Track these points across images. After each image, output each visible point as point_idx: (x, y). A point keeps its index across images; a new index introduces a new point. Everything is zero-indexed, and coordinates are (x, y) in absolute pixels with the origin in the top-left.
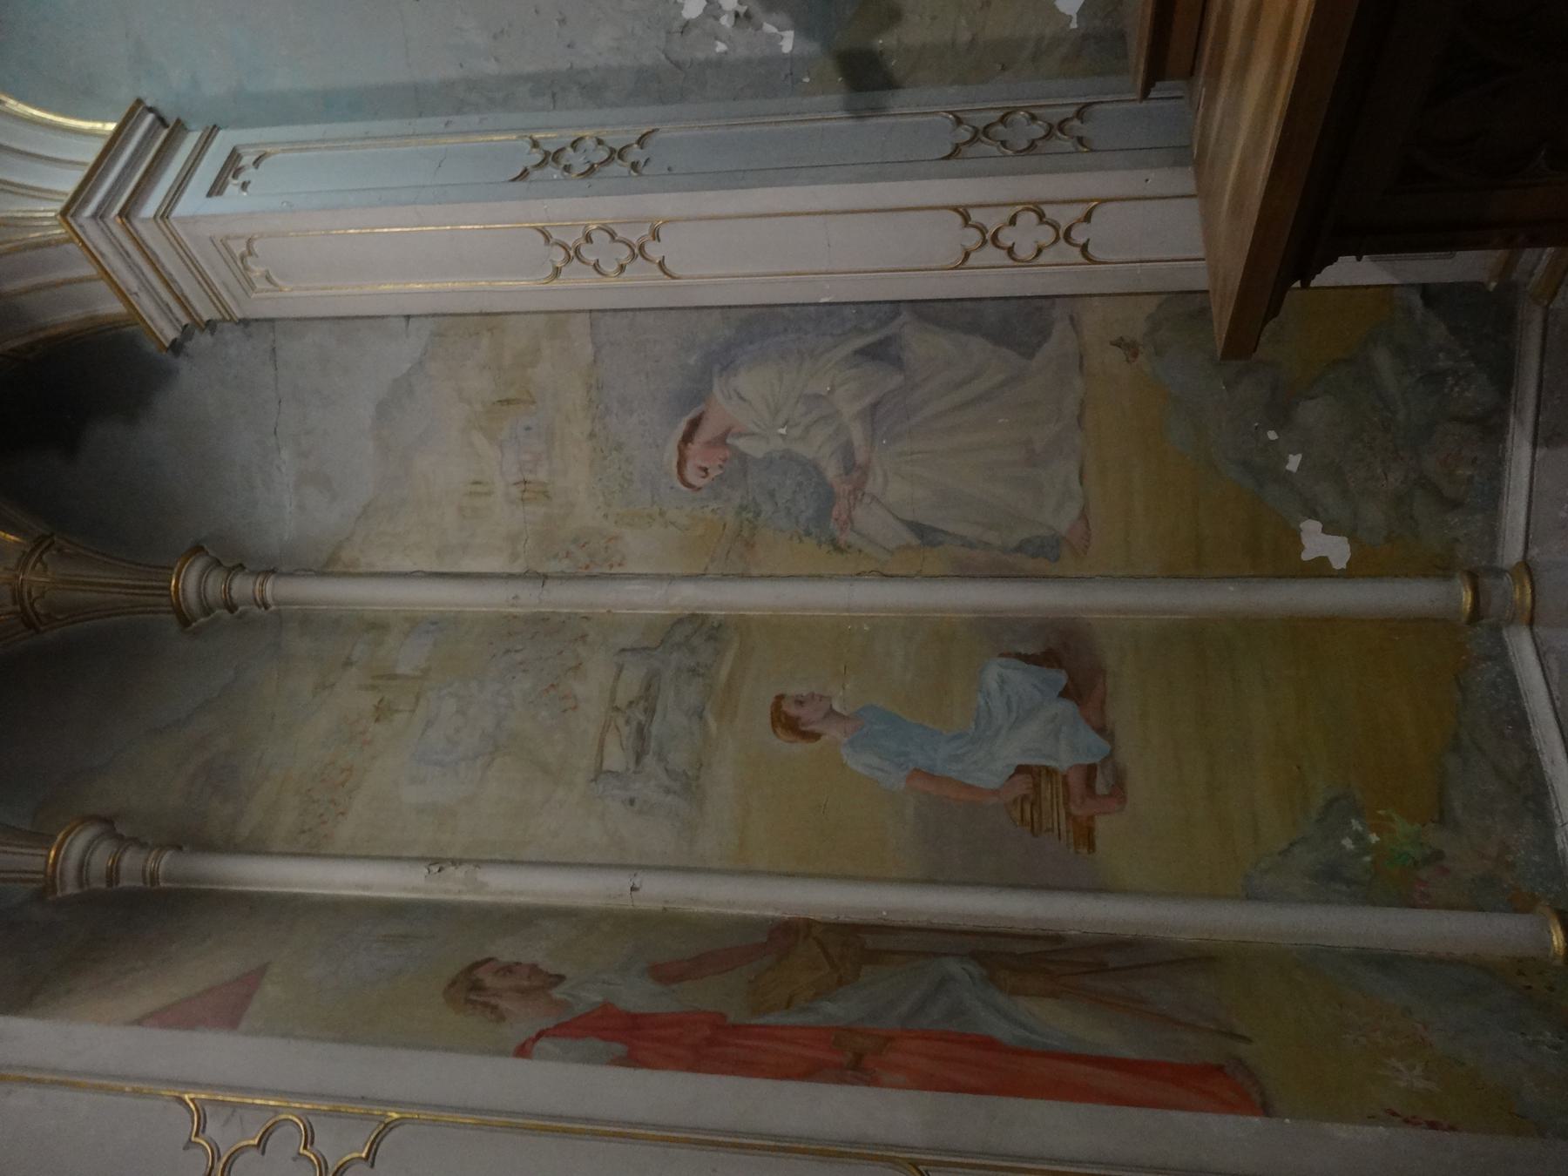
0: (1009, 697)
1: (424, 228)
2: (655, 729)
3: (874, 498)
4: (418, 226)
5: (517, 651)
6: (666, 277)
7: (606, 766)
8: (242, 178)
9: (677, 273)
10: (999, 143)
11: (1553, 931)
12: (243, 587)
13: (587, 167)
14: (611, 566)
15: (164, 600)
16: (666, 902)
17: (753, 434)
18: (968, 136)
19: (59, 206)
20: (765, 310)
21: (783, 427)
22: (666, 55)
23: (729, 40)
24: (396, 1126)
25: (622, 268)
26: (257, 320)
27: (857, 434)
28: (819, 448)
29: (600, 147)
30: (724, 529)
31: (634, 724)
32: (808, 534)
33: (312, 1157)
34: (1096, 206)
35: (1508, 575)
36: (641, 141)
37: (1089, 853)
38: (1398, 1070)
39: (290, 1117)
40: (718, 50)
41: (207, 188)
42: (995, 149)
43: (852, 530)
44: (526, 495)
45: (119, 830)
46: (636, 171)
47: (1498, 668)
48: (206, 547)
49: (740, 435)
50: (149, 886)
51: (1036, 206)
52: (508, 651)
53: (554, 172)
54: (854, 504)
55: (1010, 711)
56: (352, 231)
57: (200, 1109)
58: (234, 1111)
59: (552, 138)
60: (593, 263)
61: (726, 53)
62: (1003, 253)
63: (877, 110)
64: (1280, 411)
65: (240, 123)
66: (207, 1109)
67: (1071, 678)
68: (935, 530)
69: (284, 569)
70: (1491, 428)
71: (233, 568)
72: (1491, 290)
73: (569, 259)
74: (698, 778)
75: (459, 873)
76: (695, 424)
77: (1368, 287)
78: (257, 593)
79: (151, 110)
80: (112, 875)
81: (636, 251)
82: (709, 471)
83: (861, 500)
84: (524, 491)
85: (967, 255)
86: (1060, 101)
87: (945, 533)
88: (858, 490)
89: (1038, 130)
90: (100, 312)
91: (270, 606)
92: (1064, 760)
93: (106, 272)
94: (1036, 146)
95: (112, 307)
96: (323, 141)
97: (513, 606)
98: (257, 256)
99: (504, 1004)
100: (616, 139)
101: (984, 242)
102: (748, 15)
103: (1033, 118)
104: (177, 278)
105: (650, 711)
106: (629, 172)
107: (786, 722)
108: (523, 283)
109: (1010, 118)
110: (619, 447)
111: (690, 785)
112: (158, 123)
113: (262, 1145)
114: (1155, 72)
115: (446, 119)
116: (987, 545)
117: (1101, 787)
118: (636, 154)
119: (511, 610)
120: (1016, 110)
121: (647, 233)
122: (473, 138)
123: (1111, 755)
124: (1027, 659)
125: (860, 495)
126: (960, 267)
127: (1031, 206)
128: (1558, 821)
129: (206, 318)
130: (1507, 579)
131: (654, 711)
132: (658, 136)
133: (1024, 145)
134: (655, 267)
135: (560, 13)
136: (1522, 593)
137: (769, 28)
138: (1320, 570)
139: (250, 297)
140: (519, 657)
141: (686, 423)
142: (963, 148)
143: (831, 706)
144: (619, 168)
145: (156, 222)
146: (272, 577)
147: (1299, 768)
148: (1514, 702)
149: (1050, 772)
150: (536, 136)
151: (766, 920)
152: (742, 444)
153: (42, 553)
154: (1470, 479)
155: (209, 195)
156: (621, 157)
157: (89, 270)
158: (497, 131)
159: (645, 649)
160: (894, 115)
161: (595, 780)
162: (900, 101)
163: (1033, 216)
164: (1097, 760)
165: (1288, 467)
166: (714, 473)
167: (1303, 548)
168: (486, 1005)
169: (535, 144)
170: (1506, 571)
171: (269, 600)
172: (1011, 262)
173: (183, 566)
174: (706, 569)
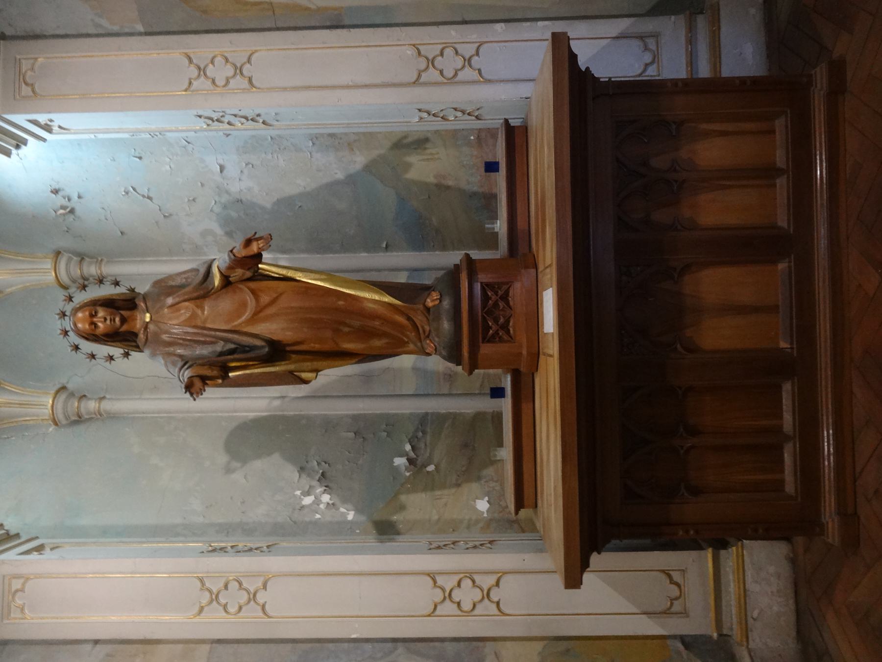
9: (271, 613)
23: (322, 514)
34: (501, 575)
40: (316, 517)
51: (471, 575)
61: (320, 519)
62: (455, 606)
102: (333, 504)
126: (432, 615)
127: (468, 575)
132: (278, 546)
135: (243, 500)
137: (342, 510)
139: (2, 621)
172: (460, 613)
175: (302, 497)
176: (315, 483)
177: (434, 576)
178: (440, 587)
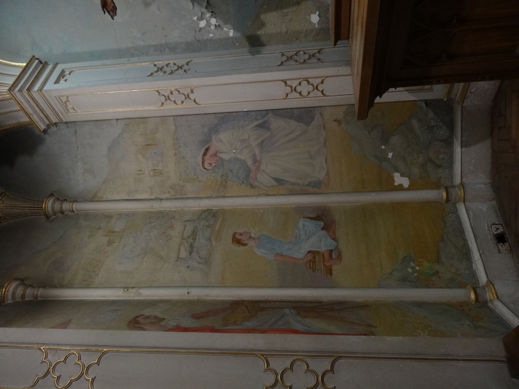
0: (306, 230)
1: (121, 92)
2: (196, 245)
3: (263, 171)
4: (119, 91)
5: (153, 222)
6: (196, 104)
7: (180, 257)
8: (65, 78)
9: (200, 103)
10: (295, 61)
11: (471, 294)
12: (66, 206)
13: (171, 71)
14: (182, 195)
15: (41, 211)
16: (199, 296)
17: (225, 152)
18: (285, 59)
19: (7, 88)
20: (227, 114)
21: (234, 150)
22: (195, 38)
23: (213, 33)
24: (106, 353)
25: (183, 102)
26: (70, 122)
27: (257, 151)
28: (245, 156)
29: (175, 66)
30: (217, 182)
31: (189, 243)
32: (243, 183)
33: (80, 363)
34: (324, 79)
35: (457, 188)
36: (187, 64)
37: (330, 276)
38: (421, 333)
39: (74, 352)
41: (54, 82)
42: (294, 63)
43: (257, 181)
44: (155, 174)
45: (26, 283)
46: (185, 72)
47: (455, 216)
48: (54, 194)
49: (221, 153)
50: (35, 299)
52: (150, 223)
53: (161, 73)
54: (257, 173)
55: (306, 234)
56: (99, 93)
57: (46, 352)
58: (56, 352)
59: (160, 64)
60: (173, 101)
61: (213, 37)
62: (298, 94)
63: (259, 52)
64: (385, 140)
65: (65, 62)
66: (48, 351)
67: (325, 224)
68: (282, 180)
69: (79, 201)
70: (449, 143)
71: (63, 200)
72: (445, 101)
73: (166, 100)
74: (209, 259)
75: (134, 290)
76: (207, 150)
77: (409, 101)
78: (71, 208)
79: (37, 59)
80: (23, 296)
81: (187, 97)
82: (212, 164)
83: (259, 171)
84: (155, 172)
85: (287, 95)
86: (313, 48)
87: (285, 181)
88: (258, 168)
89: (307, 57)
90: (21, 121)
91: (75, 212)
92: (323, 248)
93: (23, 108)
94: (306, 61)
95: (25, 119)
96: (90, 66)
97: (151, 209)
98: (70, 102)
99: (145, 327)
100: (180, 63)
101: (292, 91)
102: (219, 26)
103: (305, 53)
104: (45, 109)
105: (194, 239)
106: (184, 73)
107: (237, 241)
108: (152, 108)
109: (298, 54)
110: (183, 158)
111: (207, 261)
112: (40, 63)
113: (65, 361)
114: (337, 38)
115: (128, 59)
116: (298, 184)
117: (334, 256)
118: (186, 67)
119: (151, 210)
120: (300, 51)
121: (190, 91)
122: (136, 64)
123: (337, 246)
124: (311, 219)
125: (258, 171)
127: (305, 79)
128: (473, 260)
129: (54, 122)
130: (457, 188)
131: (195, 239)
133: (303, 61)
134: (193, 101)
136: (461, 192)
137: (225, 29)
138: (400, 188)
140: (153, 224)
141: (204, 150)
142: (284, 63)
143: (251, 235)
144: (181, 71)
145: (38, 92)
146: (75, 203)
147: (395, 248)
148: (459, 226)
149: (318, 252)
150: (156, 63)
151: (230, 300)
152: (222, 156)
153: (2, 197)
154: (444, 158)
155: (55, 83)
156: (181, 68)
157: (18, 108)
158: (143, 62)
159: (193, 220)
160: (264, 54)
161: (177, 261)
162: (266, 50)
163: (306, 82)
164: (333, 248)
165: (388, 157)
166: (213, 165)
167: (395, 181)
168: (140, 327)
169: (155, 65)
170: (456, 186)
171: (75, 210)
172: (300, 97)
173: (47, 200)
174: (212, 195)
175: (198, 21)
176: (204, 10)
177: (285, 81)
178: (289, 86)
